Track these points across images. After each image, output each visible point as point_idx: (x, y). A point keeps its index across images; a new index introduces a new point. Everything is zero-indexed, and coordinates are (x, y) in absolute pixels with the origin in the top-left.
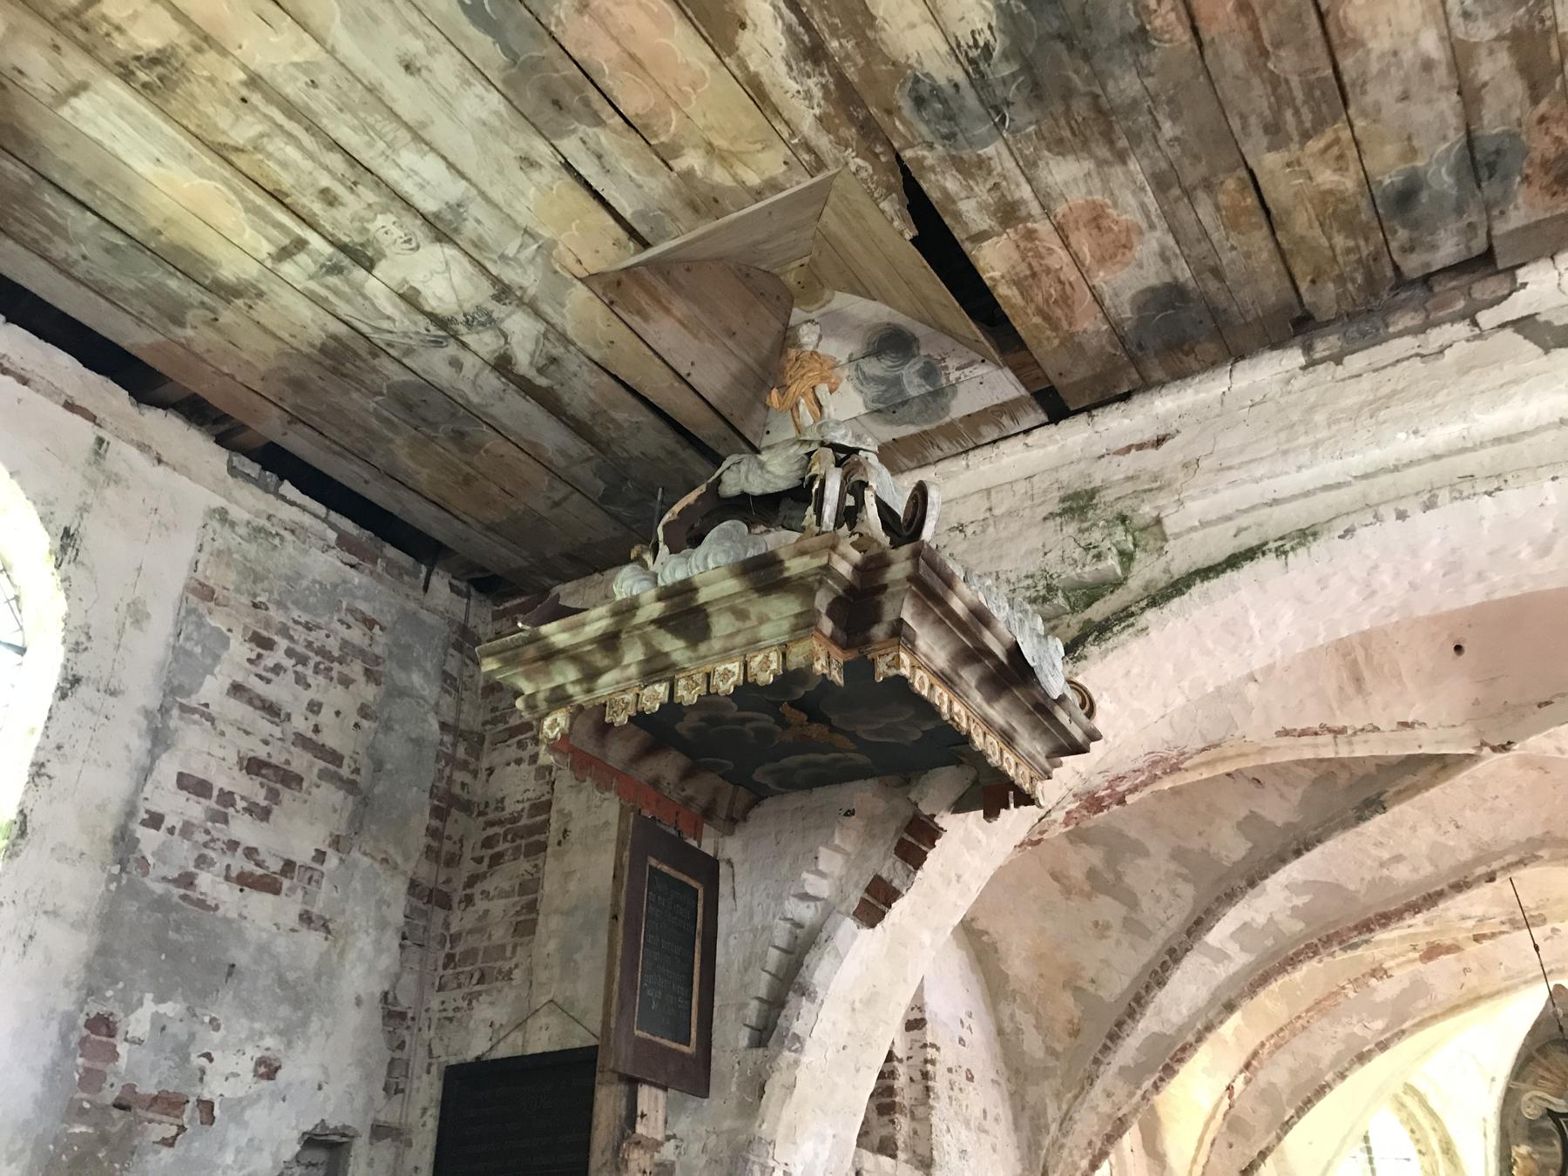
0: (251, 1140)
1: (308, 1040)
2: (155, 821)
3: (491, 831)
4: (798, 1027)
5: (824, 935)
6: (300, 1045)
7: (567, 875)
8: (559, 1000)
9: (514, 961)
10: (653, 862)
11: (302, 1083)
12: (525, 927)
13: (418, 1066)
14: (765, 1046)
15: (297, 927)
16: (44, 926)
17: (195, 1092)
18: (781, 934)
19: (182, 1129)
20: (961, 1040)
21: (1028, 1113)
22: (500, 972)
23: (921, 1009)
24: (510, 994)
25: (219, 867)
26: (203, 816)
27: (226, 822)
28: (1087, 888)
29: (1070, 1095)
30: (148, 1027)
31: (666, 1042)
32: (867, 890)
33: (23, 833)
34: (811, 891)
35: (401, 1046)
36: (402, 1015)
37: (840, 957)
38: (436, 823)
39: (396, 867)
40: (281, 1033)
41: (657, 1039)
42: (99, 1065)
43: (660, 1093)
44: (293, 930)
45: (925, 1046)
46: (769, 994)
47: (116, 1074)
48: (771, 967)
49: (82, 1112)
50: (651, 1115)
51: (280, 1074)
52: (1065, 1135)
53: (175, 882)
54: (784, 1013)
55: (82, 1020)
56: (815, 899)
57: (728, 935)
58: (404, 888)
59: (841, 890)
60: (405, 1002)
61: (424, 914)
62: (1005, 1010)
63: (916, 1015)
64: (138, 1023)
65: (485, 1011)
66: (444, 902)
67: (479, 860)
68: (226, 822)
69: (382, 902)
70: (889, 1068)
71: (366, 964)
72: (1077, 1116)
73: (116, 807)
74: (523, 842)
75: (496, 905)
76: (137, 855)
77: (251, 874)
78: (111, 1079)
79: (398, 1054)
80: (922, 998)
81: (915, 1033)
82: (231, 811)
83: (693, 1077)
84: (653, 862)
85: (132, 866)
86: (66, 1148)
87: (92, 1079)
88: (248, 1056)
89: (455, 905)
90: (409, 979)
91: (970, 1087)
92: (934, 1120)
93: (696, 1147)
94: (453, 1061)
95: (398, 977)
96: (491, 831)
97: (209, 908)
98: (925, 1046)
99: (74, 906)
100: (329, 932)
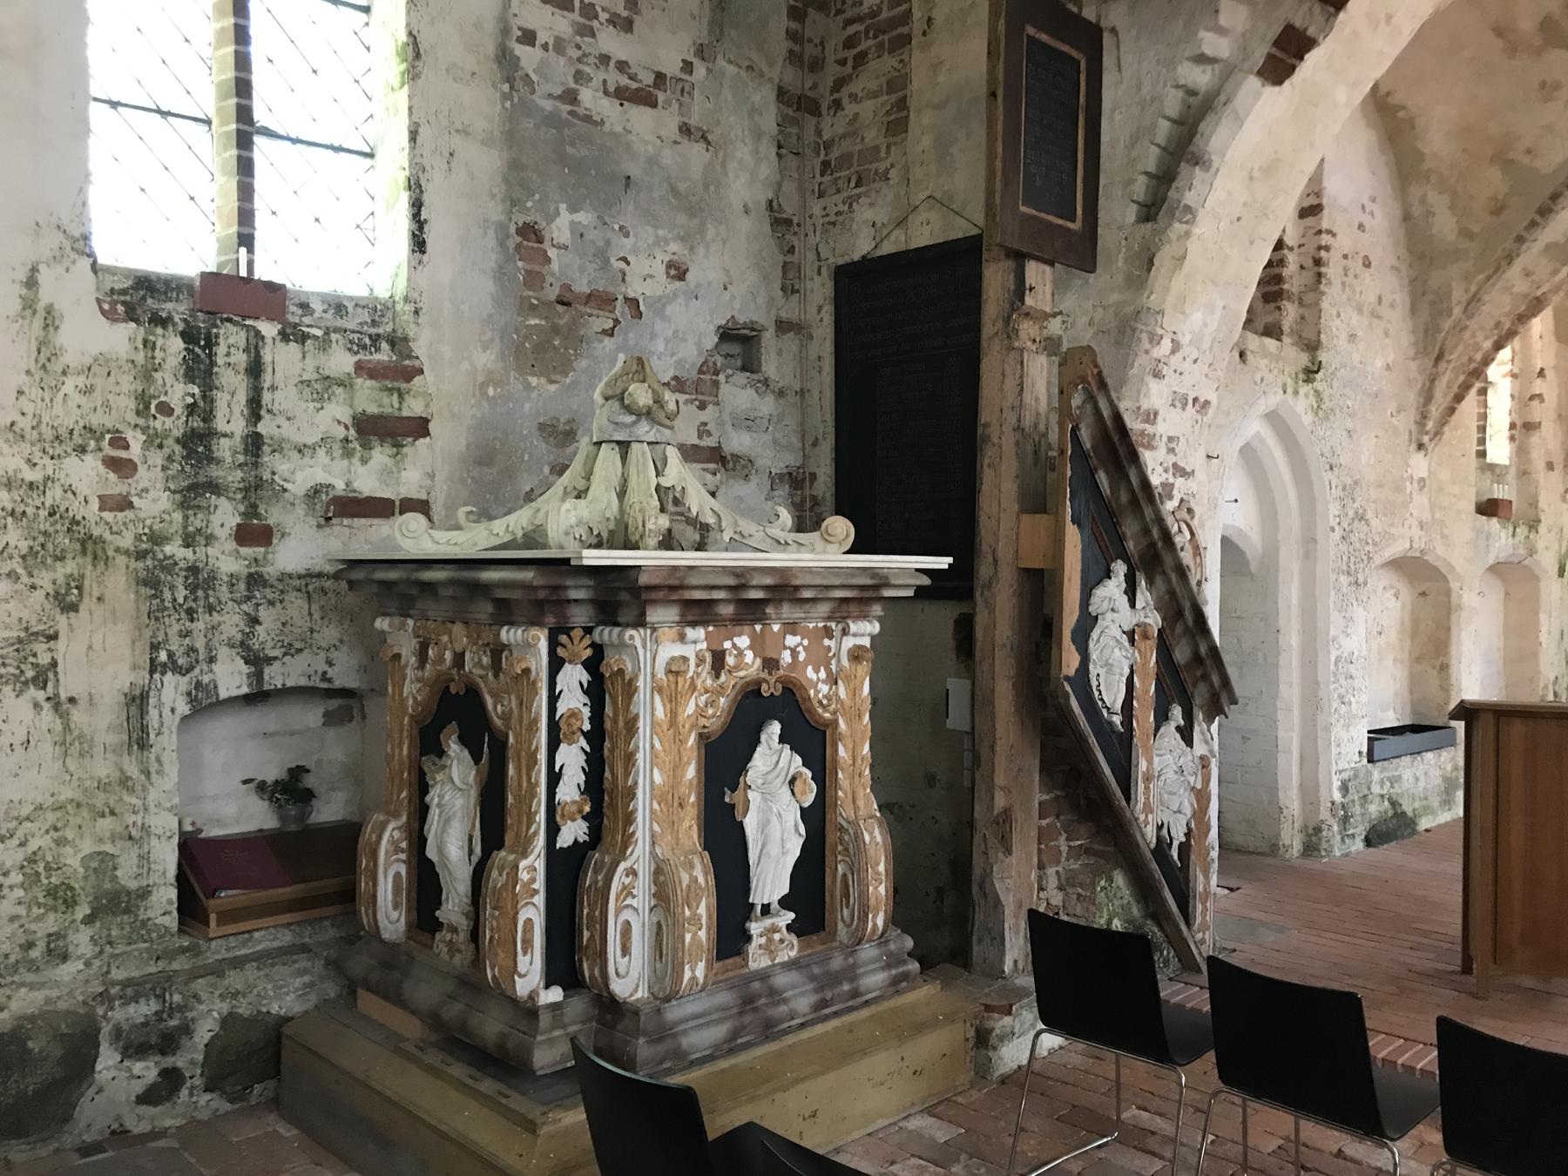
0: (676, 332)
1: (707, 247)
2: (528, 37)
3: (851, 30)
4: (1189, 198)
5: (1222, 98)
6: (701, 250)
7: (936, 67)
8: (938, 195)
9: (890, 160)
10: (1030, 30)
11: (710, 284)
12: (897, 126)
13: (809, 268)
14: (1155, 220)
15: (678, 139)
16: (457, 142)
17: (620, 291)
18: (1173, 103)
19: (617, 322)
20: (1361, 227)
21: (1430, 297)
22: (876, 173)
23: (1318, 195)
24: (888, 193)
25: (597, 82)
26: (570, 31)
27: (593, 35)
28: (1537, 42)
29: (1481, 277)
30: (569, 235)
31: (1051, 218)
32: (1276, 44)
33: (418, 55)
34: (1208, 52)
35: (791, 250)
36: (788, 222)
37: (1239, 121)
38: (794, 25)
39: (762, 75)
40: (683, 239)
41: (1043, 215)
42: (537, 268)
43: (1047, 269)
44: (675, 142)
45: (1320, 232)
46: (1158, 167)
47: (553, 275)
48: (1161, 138)
49: (533, 308)
50: (1039, 289)
51: (688, 275)
52: (1470, 317)
53: (559, 98)
54: (1174, 185)
55: (513, 229)
56: (1212, 61)
57: (1113, 111)
58: (773, 96)
59: (1244, 49)
60: (790, 209)
61: (795, 122)
62: (1415, 191)
63: (1313, 201)
64: (560, 228)
65: (865, 213)
66: (815, 111)
67: (842, 63)
68: (593, 35)
69: (754, 111)
70: (1278, 255)
71: (748, 174)
72: (1486, 298)
73: (490, 25)
74: (886, 38)
75: (865, 109)
76: (520, 73)
77: (627, 88)
78: (549, 279)
79: (789, 258)
80: (1320, 182)
81: (1310, 220)
82: (595, 23)
83: (1080, 253)
84: (1030, 30)
85: (519, 84)
86: (527, 337)
87: (534, 280)
88: (659, 260)
89: (824, 112)
90: (789, 187)
91: (1367, 273)
92: (1325, 305)
93: (1082, 321)
94: (841, 262)
95: (780, 184)
96: (851, 30)
97: (595, 123)
98: (1320, 232)
99: (480, 125)
100: (709, 143)
